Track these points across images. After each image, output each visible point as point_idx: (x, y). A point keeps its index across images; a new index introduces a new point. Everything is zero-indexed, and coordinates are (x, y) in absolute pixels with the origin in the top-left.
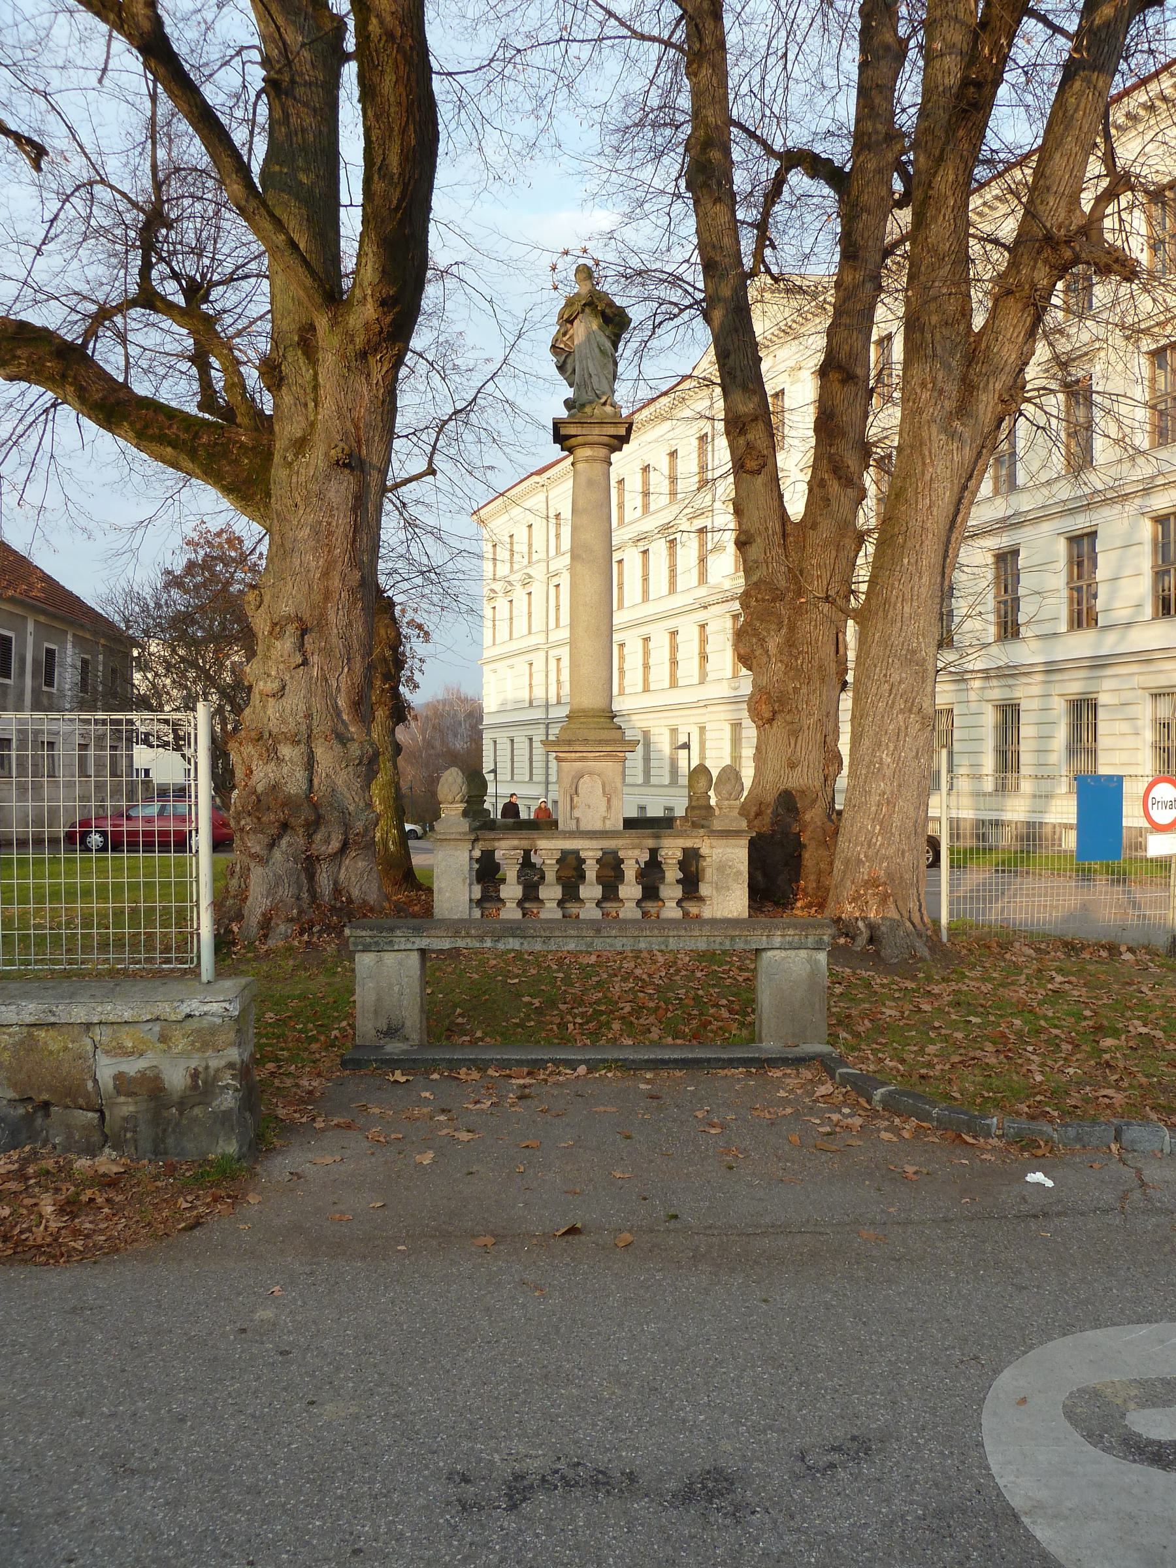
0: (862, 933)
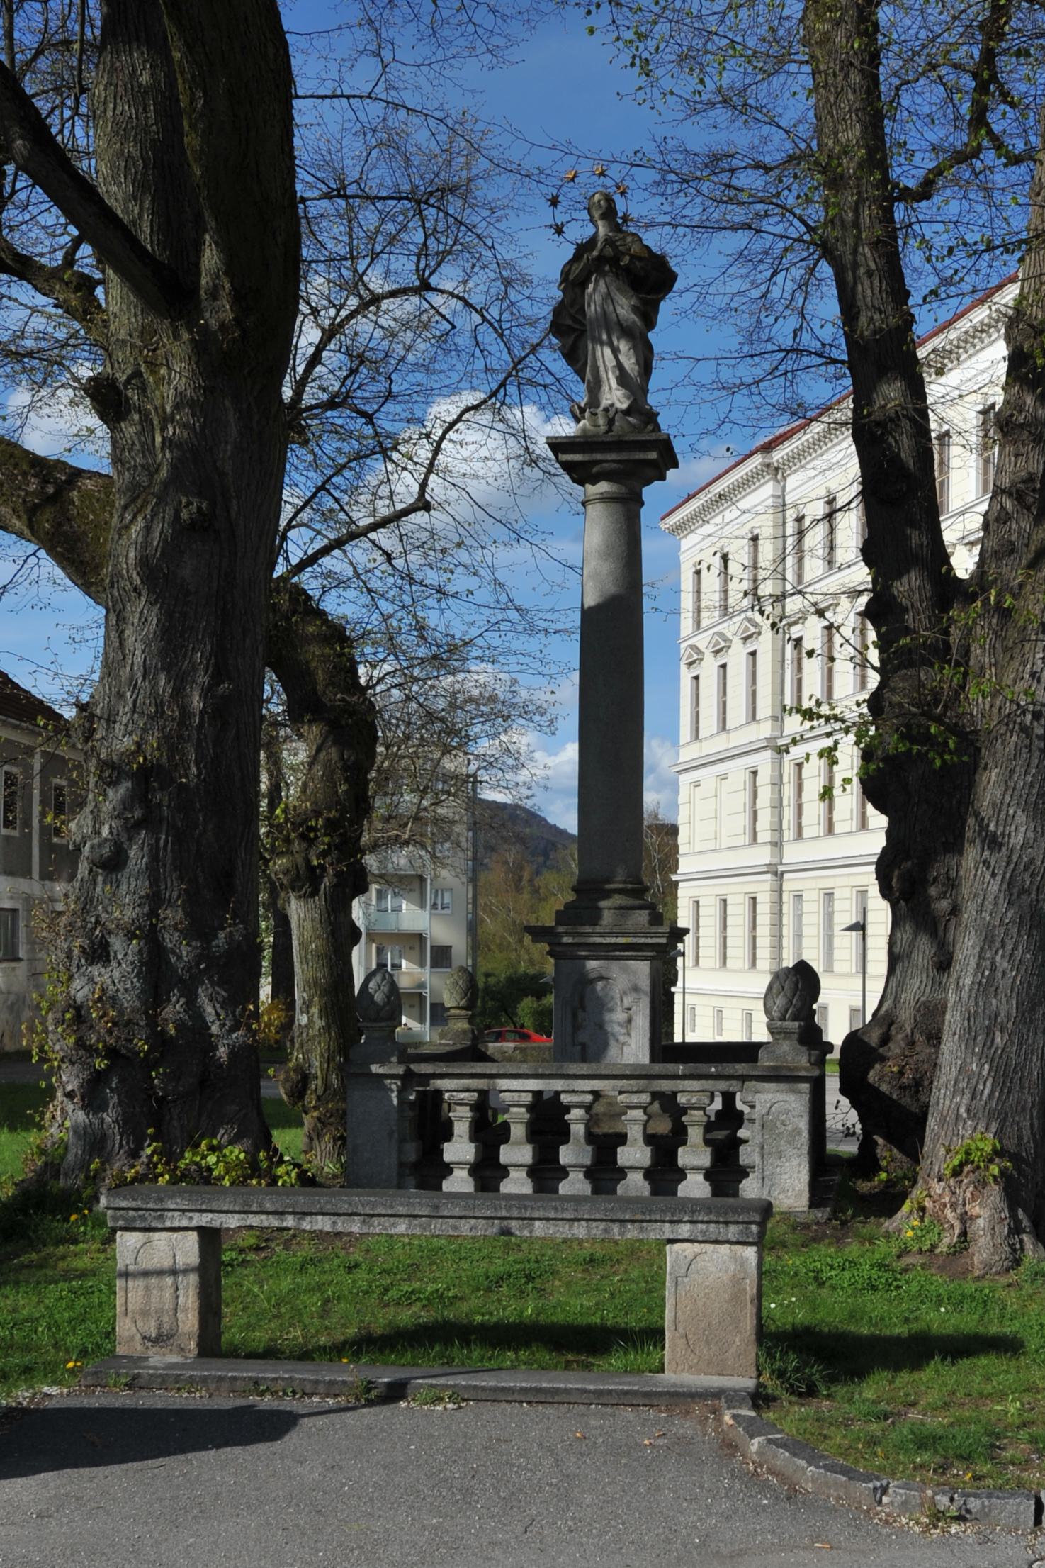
0: (952, 1226)
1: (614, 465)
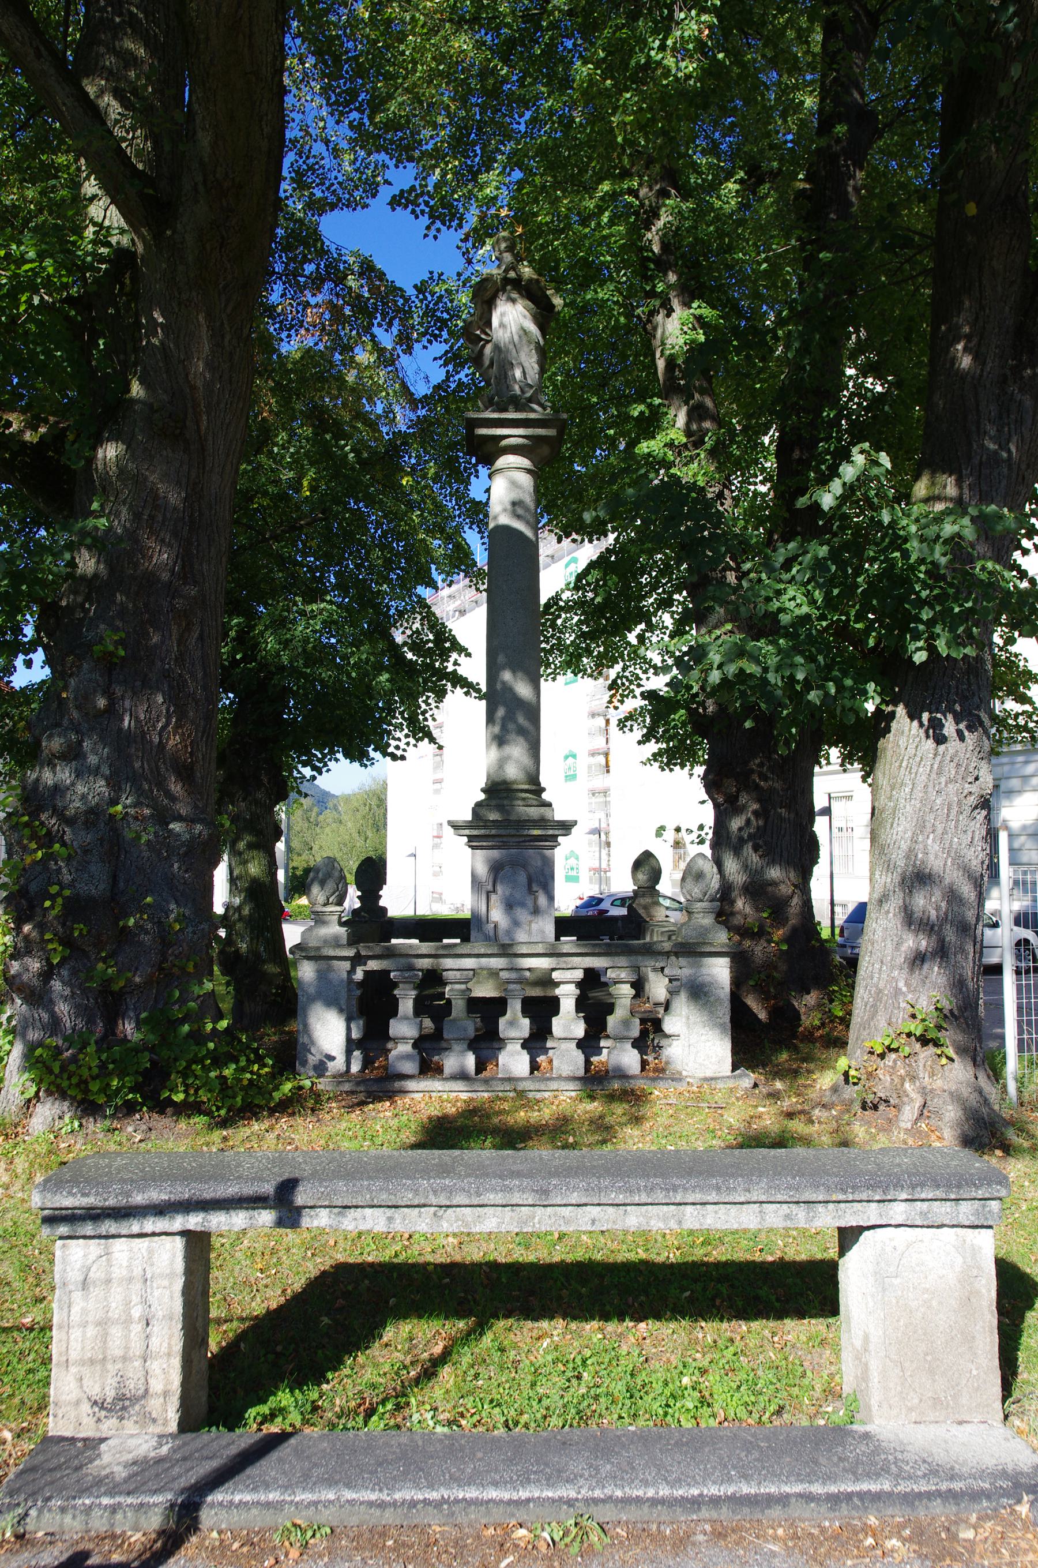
1: (520, 441)
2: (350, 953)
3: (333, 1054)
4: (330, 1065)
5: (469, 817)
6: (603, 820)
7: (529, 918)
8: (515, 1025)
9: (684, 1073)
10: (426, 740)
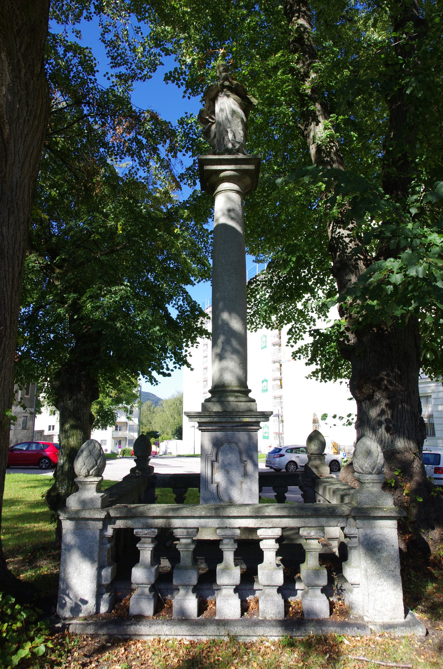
2: (102, 515)
3: (86, 598)
4: (84, 607)
5: (199, 409)
6: (280, 410)
7: (241, 479)
8: (229, 574)
9: (366, 619)
10: (185, 365)
